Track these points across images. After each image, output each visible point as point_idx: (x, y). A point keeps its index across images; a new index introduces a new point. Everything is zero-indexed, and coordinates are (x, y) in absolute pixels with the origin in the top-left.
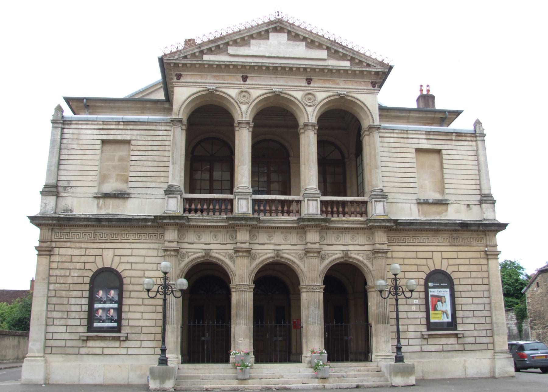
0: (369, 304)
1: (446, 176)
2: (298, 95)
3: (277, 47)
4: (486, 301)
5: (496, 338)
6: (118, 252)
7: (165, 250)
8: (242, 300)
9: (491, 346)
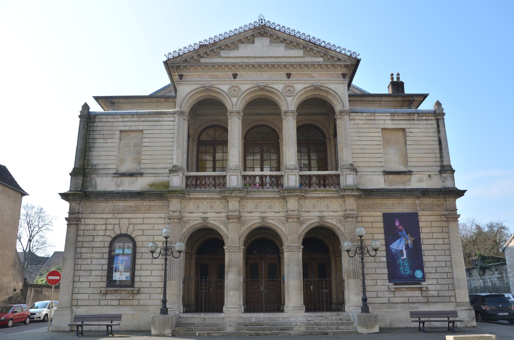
0: (343, 262)
1: (409, 151)
2: (279, 87)
4: (447, 258)
5: (456, 291)
6: (132, 221)
7: (170, 219)
8: (234, 258)
9: (453, 299)
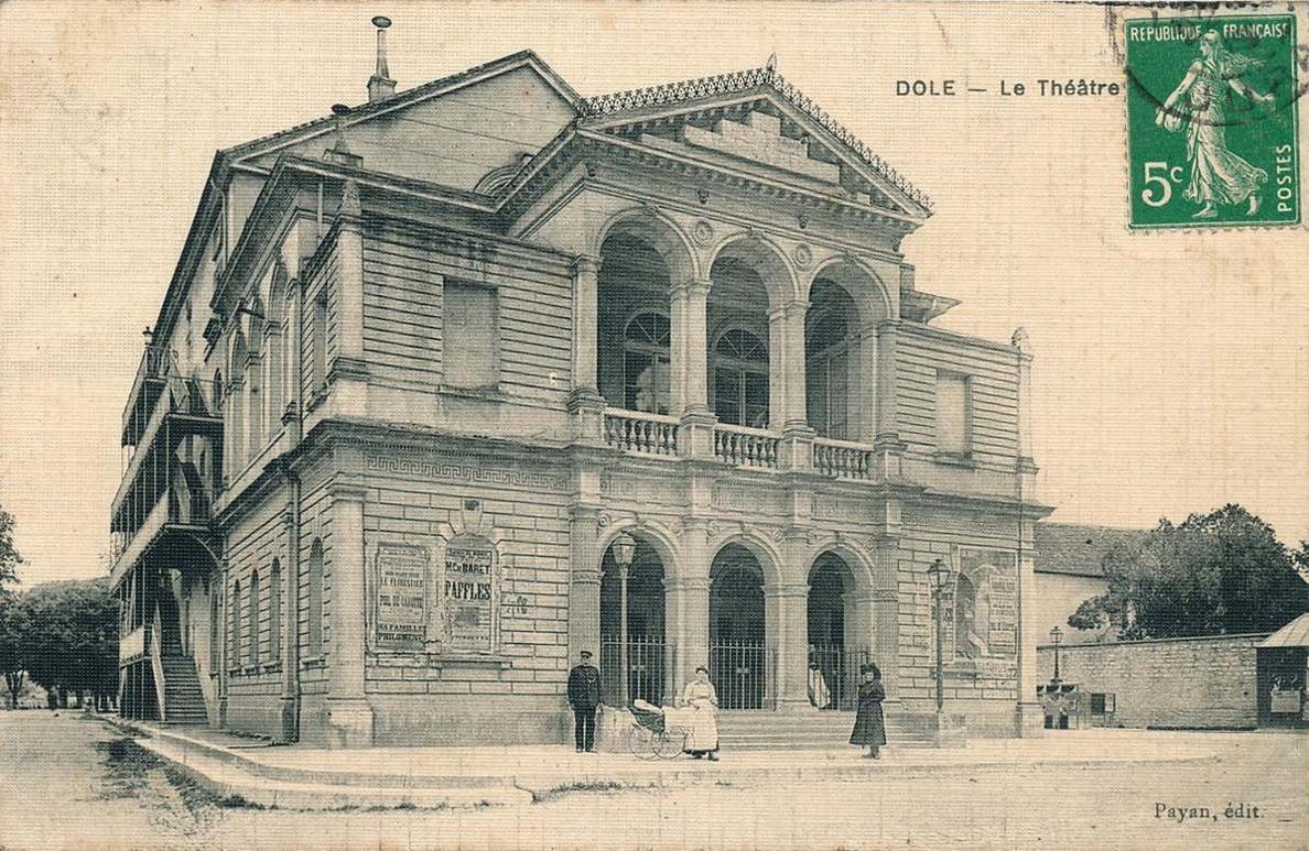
3: (757, 139)
